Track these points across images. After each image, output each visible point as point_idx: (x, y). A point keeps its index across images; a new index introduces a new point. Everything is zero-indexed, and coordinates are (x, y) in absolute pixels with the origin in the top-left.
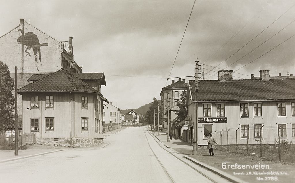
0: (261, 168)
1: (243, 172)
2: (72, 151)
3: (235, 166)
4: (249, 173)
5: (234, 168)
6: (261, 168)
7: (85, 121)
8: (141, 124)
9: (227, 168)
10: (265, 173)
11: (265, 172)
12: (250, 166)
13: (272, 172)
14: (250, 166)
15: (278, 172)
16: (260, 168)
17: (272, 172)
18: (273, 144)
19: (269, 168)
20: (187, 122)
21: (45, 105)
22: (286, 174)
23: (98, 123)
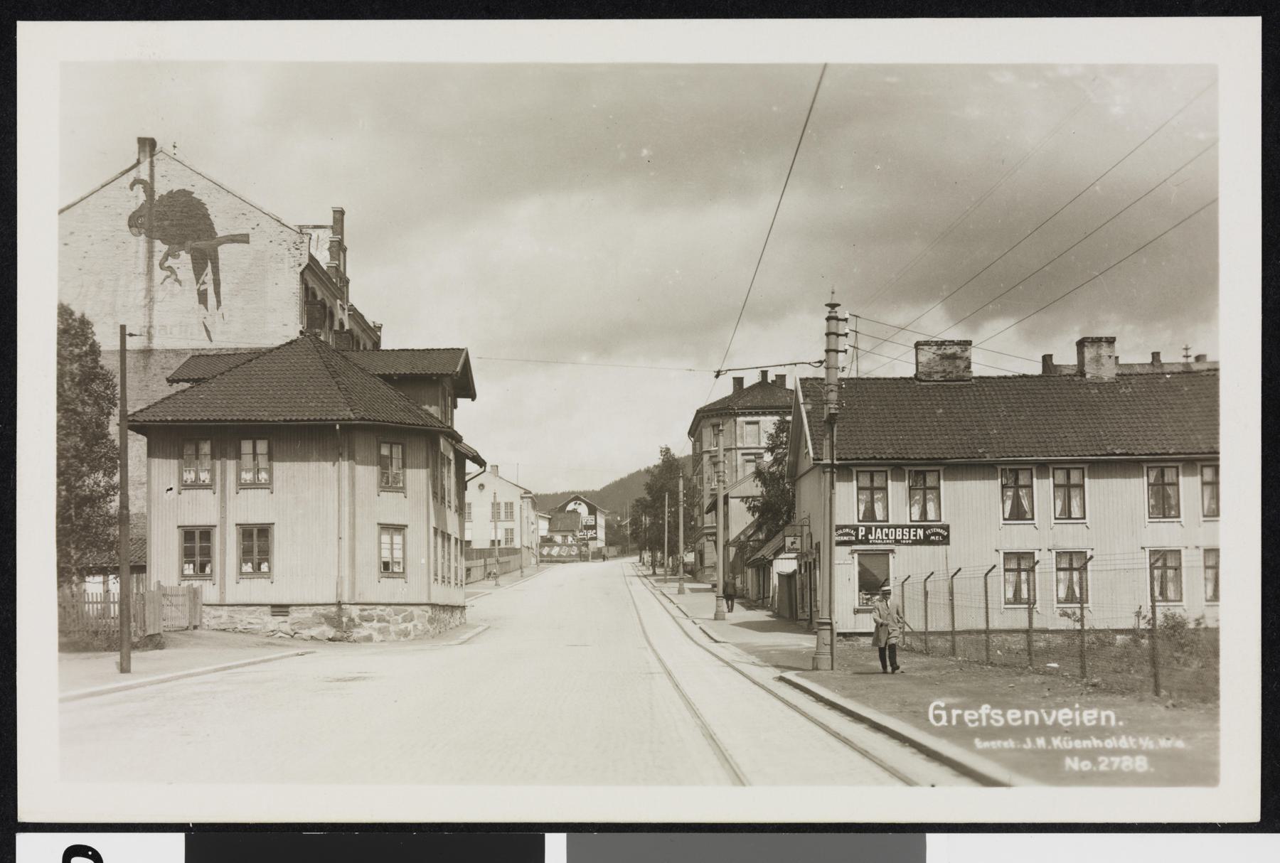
0: (1082, 722)
19: (1113, 722)
22: (1180, 744)
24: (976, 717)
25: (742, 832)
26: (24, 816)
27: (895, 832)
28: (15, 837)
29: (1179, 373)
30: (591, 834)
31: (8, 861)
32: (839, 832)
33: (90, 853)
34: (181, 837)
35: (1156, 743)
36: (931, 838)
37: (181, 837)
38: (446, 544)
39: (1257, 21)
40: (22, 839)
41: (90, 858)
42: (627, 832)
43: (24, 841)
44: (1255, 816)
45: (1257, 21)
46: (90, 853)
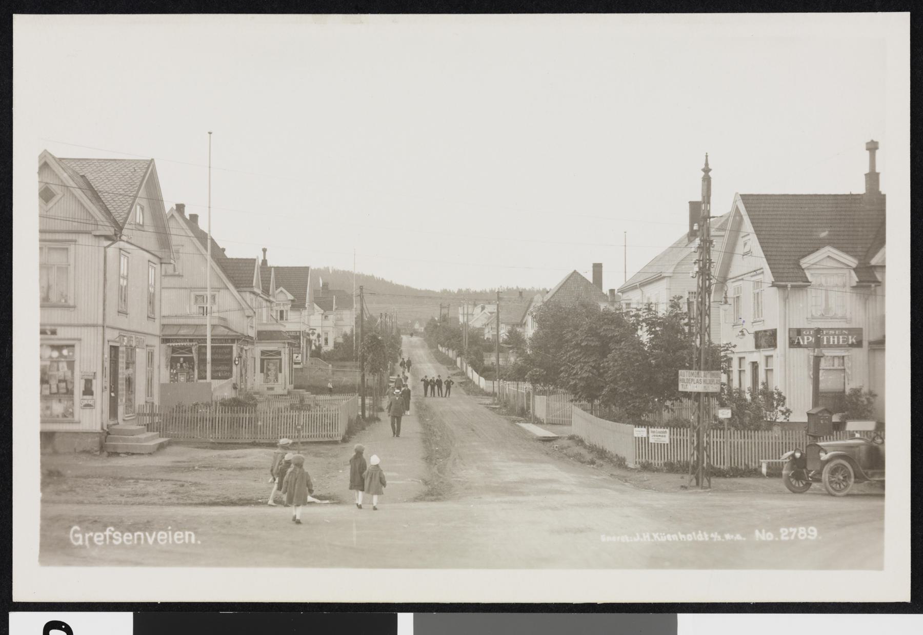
0: (173, 541)
1: (819, 531)
2: (329, 493)
3: (105, 536)
4: (641, 536)
5: (131, 543)
6: (173, 541)
7: (518, 385)
8: (791, 341)
9: (84, 541)
10: (683, 536)
11: (682, 533)
12: (145, 535)
13: (700, 532)
14: (145, 535)
15: (716, 533)
16: (170, 542)
17: (702, 533)
18: (250, 443)
19: (193, 541)
20: (297, 357)
21: (291, 358)
22: (738, 537)
23: (440, 391)
24: (182, 536)
25: (542, 612)
26: (17, 597)
27: (655, 612)
28: (8, 615)
29: (212, 398)
30: (431, 613)
31: (4, 633)
32: (614, 612)
33: (63, 627)
34: (129, 616)
35: (723, 537)
36: (682, 618)
37: (129, 616)
38: (787, 304)
39: (905, 17)
40: (15, 618)
41: (64, 631)
42: (458, 612)
43: (15, 618)
44: (905, 596)
45: (905, 17)
46: (63, 627)
